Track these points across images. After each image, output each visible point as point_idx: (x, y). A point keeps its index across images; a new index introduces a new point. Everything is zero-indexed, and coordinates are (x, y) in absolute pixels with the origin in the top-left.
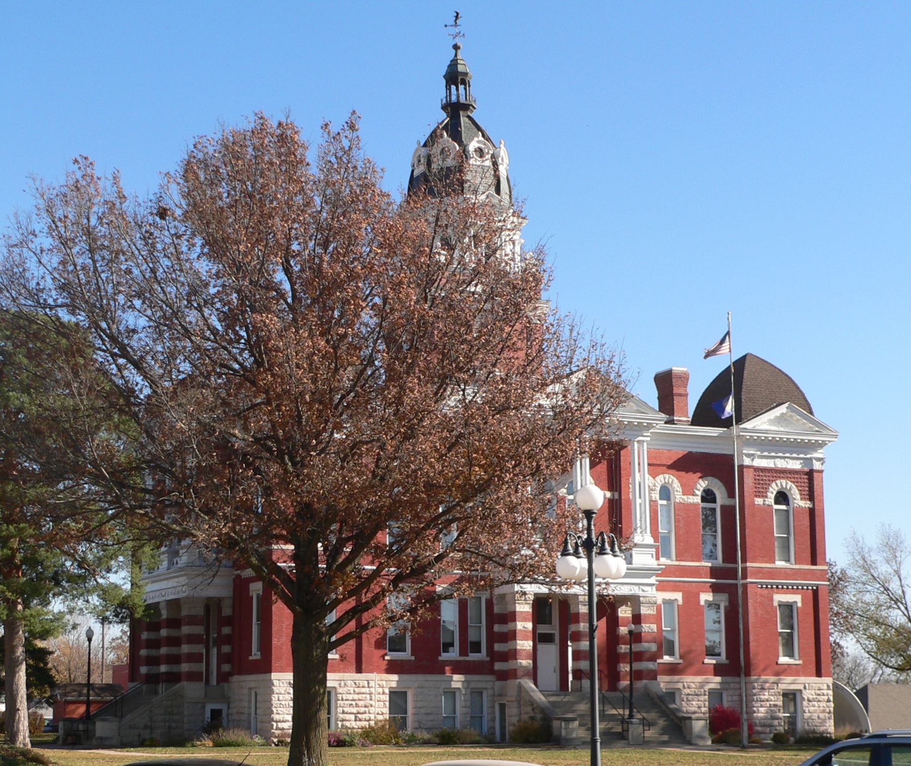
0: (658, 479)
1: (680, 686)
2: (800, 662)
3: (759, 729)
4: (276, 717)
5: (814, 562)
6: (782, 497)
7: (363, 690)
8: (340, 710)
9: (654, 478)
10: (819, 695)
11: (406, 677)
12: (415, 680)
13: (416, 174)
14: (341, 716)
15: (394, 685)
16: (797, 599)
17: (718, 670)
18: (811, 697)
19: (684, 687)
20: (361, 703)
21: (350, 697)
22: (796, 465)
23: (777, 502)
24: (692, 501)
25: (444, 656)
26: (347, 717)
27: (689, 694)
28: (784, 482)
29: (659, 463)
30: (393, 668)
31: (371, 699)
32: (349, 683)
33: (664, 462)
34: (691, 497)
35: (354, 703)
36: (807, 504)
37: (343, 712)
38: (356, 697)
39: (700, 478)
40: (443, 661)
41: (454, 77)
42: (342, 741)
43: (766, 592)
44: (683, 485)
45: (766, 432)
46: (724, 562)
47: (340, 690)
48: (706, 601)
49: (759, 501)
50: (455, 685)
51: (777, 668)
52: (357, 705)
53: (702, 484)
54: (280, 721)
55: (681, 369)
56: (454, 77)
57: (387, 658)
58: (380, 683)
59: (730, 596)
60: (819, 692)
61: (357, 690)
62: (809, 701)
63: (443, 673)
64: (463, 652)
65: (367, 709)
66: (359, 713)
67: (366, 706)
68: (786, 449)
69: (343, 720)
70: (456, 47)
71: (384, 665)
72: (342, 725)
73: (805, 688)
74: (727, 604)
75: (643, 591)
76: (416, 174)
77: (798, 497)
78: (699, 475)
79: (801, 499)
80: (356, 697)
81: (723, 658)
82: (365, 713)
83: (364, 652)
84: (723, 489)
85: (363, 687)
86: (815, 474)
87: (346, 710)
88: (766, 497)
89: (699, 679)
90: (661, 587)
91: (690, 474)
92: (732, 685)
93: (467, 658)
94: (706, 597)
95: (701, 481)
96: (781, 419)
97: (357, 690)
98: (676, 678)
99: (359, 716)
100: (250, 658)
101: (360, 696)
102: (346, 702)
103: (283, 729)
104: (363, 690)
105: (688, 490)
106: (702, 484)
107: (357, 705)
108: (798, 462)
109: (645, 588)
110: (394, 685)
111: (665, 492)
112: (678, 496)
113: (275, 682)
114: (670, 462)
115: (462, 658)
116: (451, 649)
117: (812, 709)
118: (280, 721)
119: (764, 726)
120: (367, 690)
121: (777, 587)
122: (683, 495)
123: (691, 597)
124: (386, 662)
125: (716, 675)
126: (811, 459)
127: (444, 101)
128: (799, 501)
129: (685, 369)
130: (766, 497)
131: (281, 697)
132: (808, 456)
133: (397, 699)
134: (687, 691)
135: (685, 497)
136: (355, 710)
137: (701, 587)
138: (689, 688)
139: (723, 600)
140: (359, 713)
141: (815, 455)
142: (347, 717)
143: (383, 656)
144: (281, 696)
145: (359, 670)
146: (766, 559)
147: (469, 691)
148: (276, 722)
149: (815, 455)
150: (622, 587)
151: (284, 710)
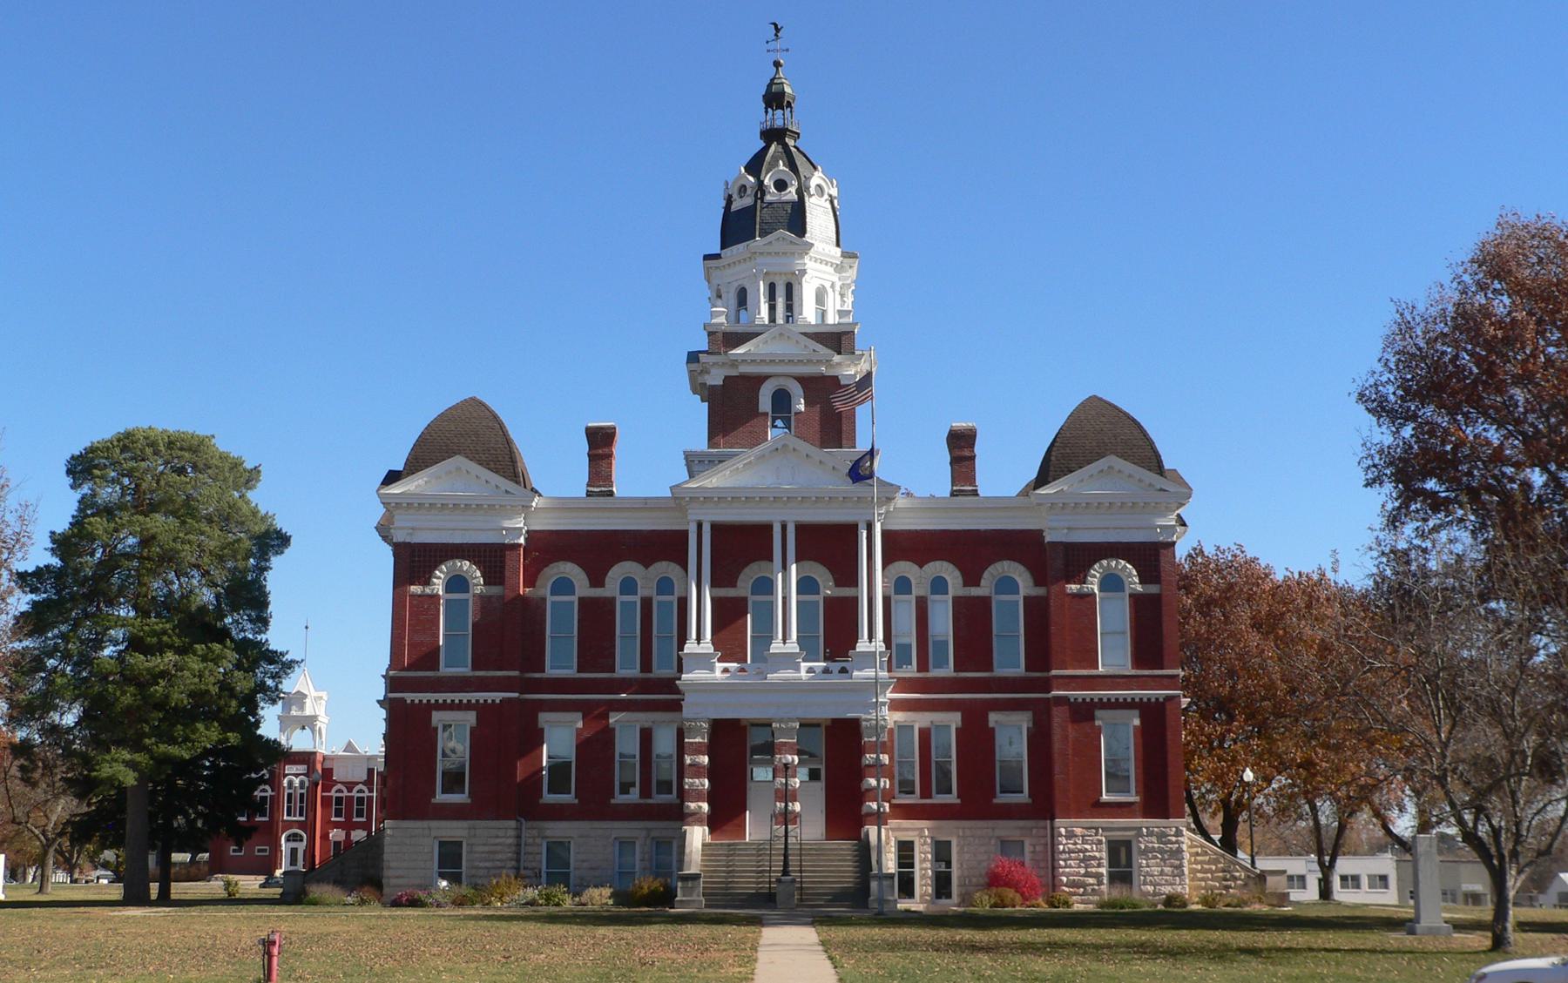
13: (734, 207)
23: (448, 589)
41: (775, 99)
46: (1028, 669)
49: (1073, 588)
56: (775, 99)
70: (777, 64)
76: (734, 207)
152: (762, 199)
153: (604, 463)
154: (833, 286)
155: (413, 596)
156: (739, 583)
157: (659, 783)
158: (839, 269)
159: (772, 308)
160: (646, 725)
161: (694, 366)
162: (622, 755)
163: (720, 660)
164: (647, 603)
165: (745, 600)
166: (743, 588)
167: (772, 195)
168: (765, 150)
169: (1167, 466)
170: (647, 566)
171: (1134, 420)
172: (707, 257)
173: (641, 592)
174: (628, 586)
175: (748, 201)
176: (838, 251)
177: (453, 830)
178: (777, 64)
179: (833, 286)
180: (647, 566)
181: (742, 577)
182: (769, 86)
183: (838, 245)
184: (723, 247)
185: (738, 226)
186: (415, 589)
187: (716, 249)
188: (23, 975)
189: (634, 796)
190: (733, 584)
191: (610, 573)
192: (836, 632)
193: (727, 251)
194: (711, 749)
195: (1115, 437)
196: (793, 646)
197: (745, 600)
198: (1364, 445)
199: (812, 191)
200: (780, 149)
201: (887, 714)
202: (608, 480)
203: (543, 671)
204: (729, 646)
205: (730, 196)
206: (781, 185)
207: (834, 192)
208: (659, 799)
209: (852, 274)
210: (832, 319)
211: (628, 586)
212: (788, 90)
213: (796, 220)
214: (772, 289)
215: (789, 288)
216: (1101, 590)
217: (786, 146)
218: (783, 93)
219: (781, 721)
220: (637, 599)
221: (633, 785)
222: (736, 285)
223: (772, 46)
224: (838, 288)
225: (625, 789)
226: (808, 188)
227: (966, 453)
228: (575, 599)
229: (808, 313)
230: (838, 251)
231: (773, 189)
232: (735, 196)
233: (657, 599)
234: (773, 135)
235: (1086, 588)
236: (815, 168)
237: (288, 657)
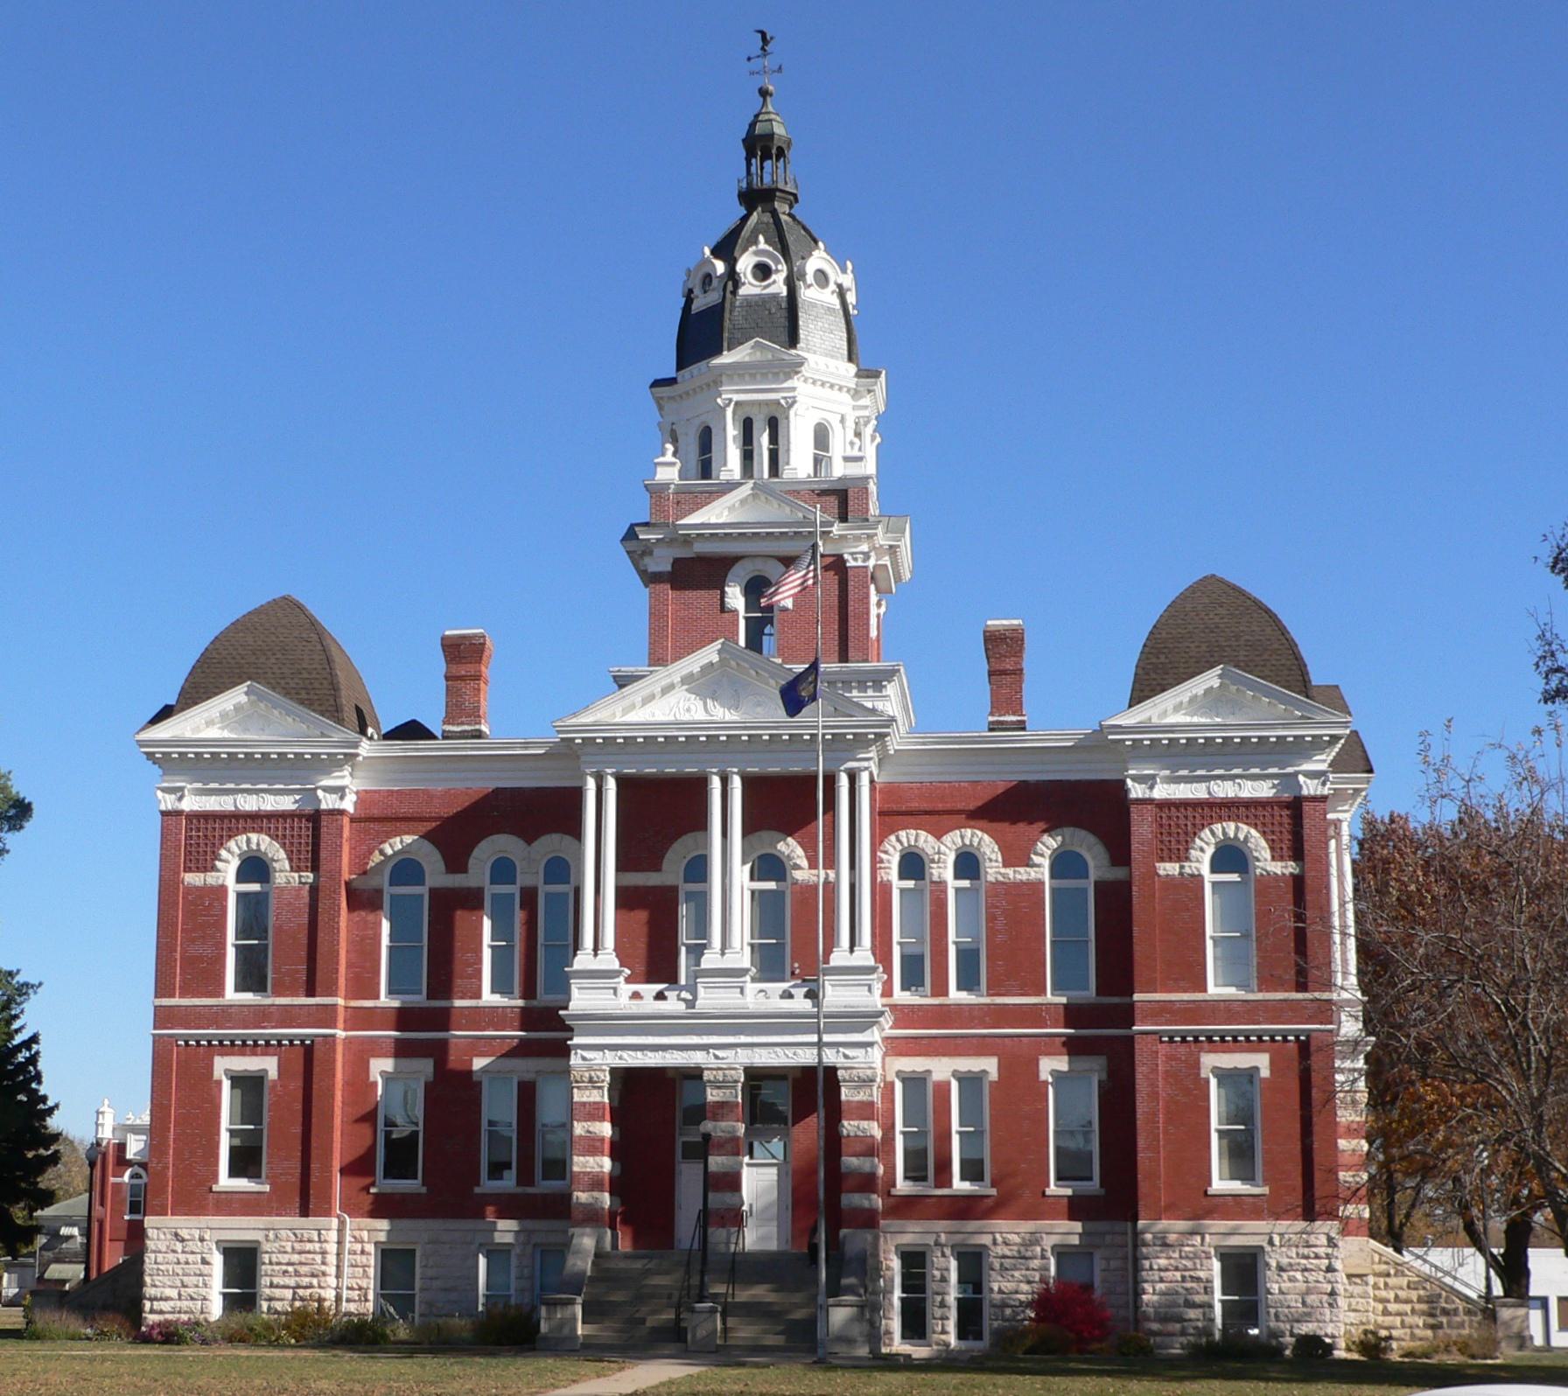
0: (947, 839)
1: (986, 1240)
2: (1265, 1190)
3: (1155, 1326)
4: (149, 1291)
5: (1302, 987)
6: (254, 867)
7: (309, 1246)
8: (265, 1281)
9: (939, 837)
10: (1307, 1257)
11: (397, 1221)
12: (419, 1232)
13: (697, 306)
14: (267, 1291)
15: (382, 1237)
16: (269, 1065)
17: (1076, 1208)
18: (1285, 1261)
19: (995, 1243)
20: (303, 1269)
21: (284, 1258)
22: (287, 803)
23: (242, 876)
24: (1024, 878)
25: (487, 1186)
26: (277, 1292)
27: (1004, 1257)
28: (1231, 827)
29: (948, 806)
30: (382, 1207)
31: (324, 1263)
32: (283, 1233)
33: (960, 806)
34: (1022, 870)
35: (290, 1269)
36: (1287, 868)
37: (272, 1286)
38: (295, 1258)
39: (1044, 831)
40: (484, 1195)
41: (760, 146)
42: (173, 1334)
43: (1183, 1049)
44: (1004, 849)
45: (1171, 728)
46: (1098, 994)
47: (266, 1247)
48: (1054, 1073)
49: (1169, 869)
50: (500, 1238)
51: (1205, 1202)
52: (297, 1273)
53: (1049, 844)
54: (156, 1299)
55: (1005, 622)
56: (760, 146)
57: (373, 1190)
58: (357, 1233)
59: (1110, 1060)
60: (1306, 1251)
61: (298, 1246)
62: (1281, 1269)
63: (482, 1216)
64: (525, 1177)
65: (315, 1281)
66: (299, 1287)
67: (313, 1275)
68: (1267, 757)
69: (270, 1299)
71: (367, 1201)
72: (269, 1308)
73: (1271, 1243)
74: (1104, 1076)
75: (846, 1057)
76: (697, 306)
77: (1267, 854)
78: (1042, 825)
79: (1273, 858)
80: (295, 1258)
81: (1094, 1186)
82: (311, 1286)
83: (313, 1179)
84: (1100, 849)
85: (310, 1241)
86: (1307, 807)
87: (276, 1281)
88: (1188, 859)
89: (1027, 1226)
90: (896, 1047)
91: (1022, 826)
92: (1108, 1238)
93: (530, 1190)
94: (1051, 1065)
95: (1046, 838)
96: (1211, 700)
97: (298, 1246)
98: (972, 1225)
99: (301, 1292)
100: (477, 1190)
101: (303, 1258)
102: (277, 1268)
103: (161, 1312)
104: (309, 1246)
105: (1016, 855)
106: (1049, 844)
107: (297, 1273)
108: (1269, 783)
109: (720, 1053)
110: (382, 1237)
111: (968, 864)
112: (994, 868)
113: (150, 1232)
114: (972, 805)
115: (520, 1190)
116: (506, 1173)
117: (1286, 1285)
118: (156, 1299)
119: (1164, 1319)
120: (317, 1246)
121: (1235, 1040)
122: (1005, 866)
123: (1019, 1067)
124: (370, 1199)
125: (1072, 1218)
126: (1296, 774)
127: (744, 185)
128: (1268, 862)
129: (1015, 622)
130: (1188, 859)
131: (160, 1258)
132: (1290, 770)
133: (394, 1263)
134: (1000, 1250)
135: (1010, 871)
136: (291, 1282)
137: (1047, 1046)
138: (1006, 1243)
139: (1095, 1070)
140: (299, 1287)
141: (1306, 767)
142: (277, 1292)
143: (366, 1189)
144: (160, 1256)
145: (305, 1212)
146: (1182, 984)
147: (529, 1249)
148: (151, 1300)
149: (1306, 767)
150: (799, 1051)
151: (165, 1280)
152: (734, 293)
153: (467, 688)
154: (842, 420)
155: (190, 890)
156: (665, 865)
157: (546, 1162)
158: (856, 394)
159: (748, 456)
160: (528, 1077)
161: (632, 545)
162: (491, 1123)
163: (628, 980)
164: (529, 898)
165: (674, 890)
166: (671, 872)
167: (750, 287)
168: (745, 219)
169: (1317, 678)
170: (529, 841)
171: (1268, 611)
172: (657, 383)
173: (523, 880)
174: (503, 870)
175: (713, 298)
176: (852, 368)
177: (243, 1229)
178: (764, 93)
179: (842, 420)
180: (529, 841)
181: (669, 855)
182: (752, 125)
183: (850, 359)
184: (681, 364)
185: (701, 334)
186: (193, 879)
187: (670, 372)
188: (982, 1392)
189: (508, 1183)
190: (657, 867)
191: (476, 852)
192: (792, 940)
193: (686, 372)
194: (618, 1115)
195: (1237, 637)
196: (741, 957)
197: (674, 890)
198: (1542, 637)
199: (810, 278)
200: (767, 218)
201: (869, 1063)
202: (475, 715)
203: (1205, 990)
204: (657, 953)
205: (691, 291)
206: (763, 271)
207: (848, 280)
208: (544, 1186)
209: (877, 398)
210: (839, 470)
211: (503, 870)
212: (779, 130)
213: (785, 322)
214: (747, 428)
215: (774, 425)
216: (1052, 877)
217: (774, 213)
218: (770, 136)
219: (846, 1069)
220: (514, 890)
221: (508, 1166)
222: (697, 422)
223: (757, 64)
224: (850, 425)
225: (497, 1170)
226: (803, 276)
227: (1008, 665)
228: (423, 890)
229: (800, 464)
230: (852, 368)
231: (750, 278)
232: (697, 291)
233: (543, 890)
234: (754, 197)
235: (1189, 868)
236: (816, 242)
237: (20, 979)
